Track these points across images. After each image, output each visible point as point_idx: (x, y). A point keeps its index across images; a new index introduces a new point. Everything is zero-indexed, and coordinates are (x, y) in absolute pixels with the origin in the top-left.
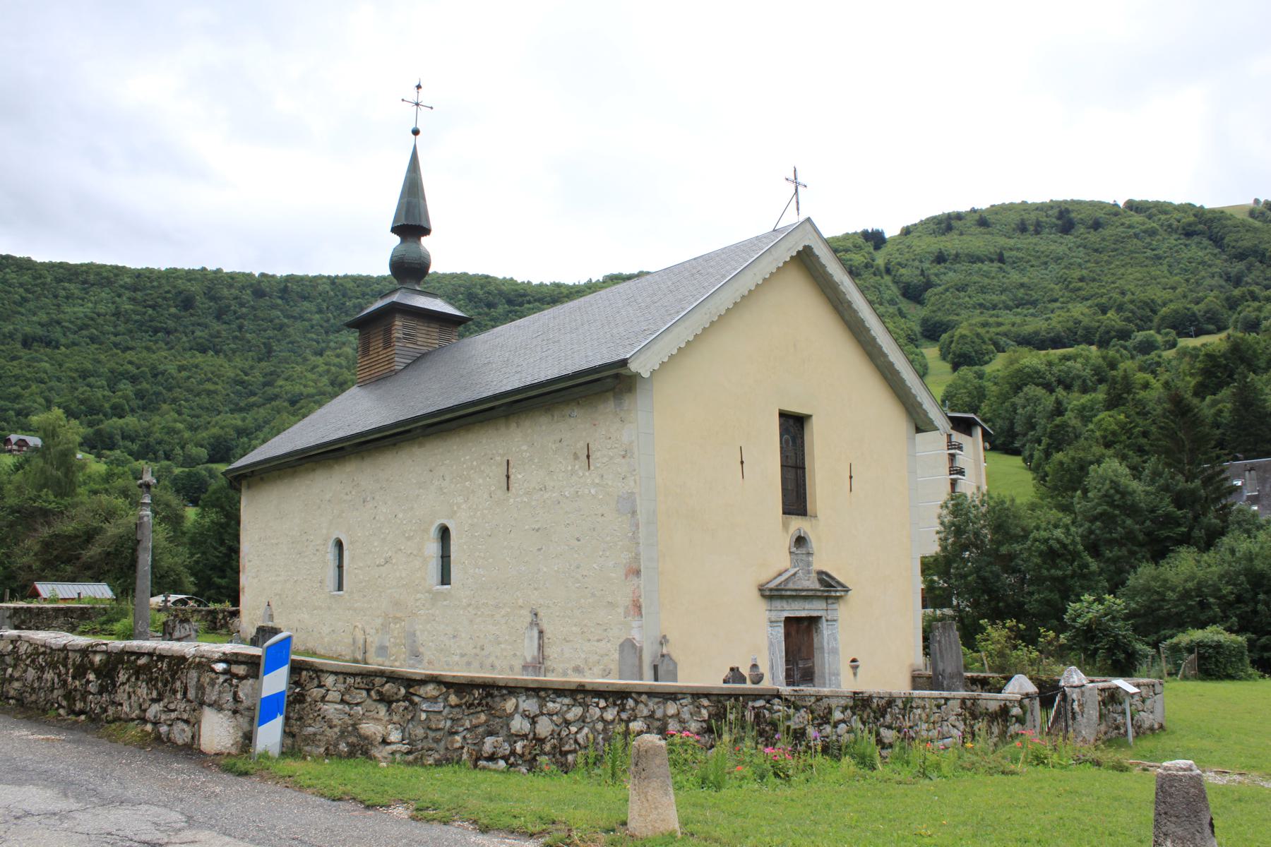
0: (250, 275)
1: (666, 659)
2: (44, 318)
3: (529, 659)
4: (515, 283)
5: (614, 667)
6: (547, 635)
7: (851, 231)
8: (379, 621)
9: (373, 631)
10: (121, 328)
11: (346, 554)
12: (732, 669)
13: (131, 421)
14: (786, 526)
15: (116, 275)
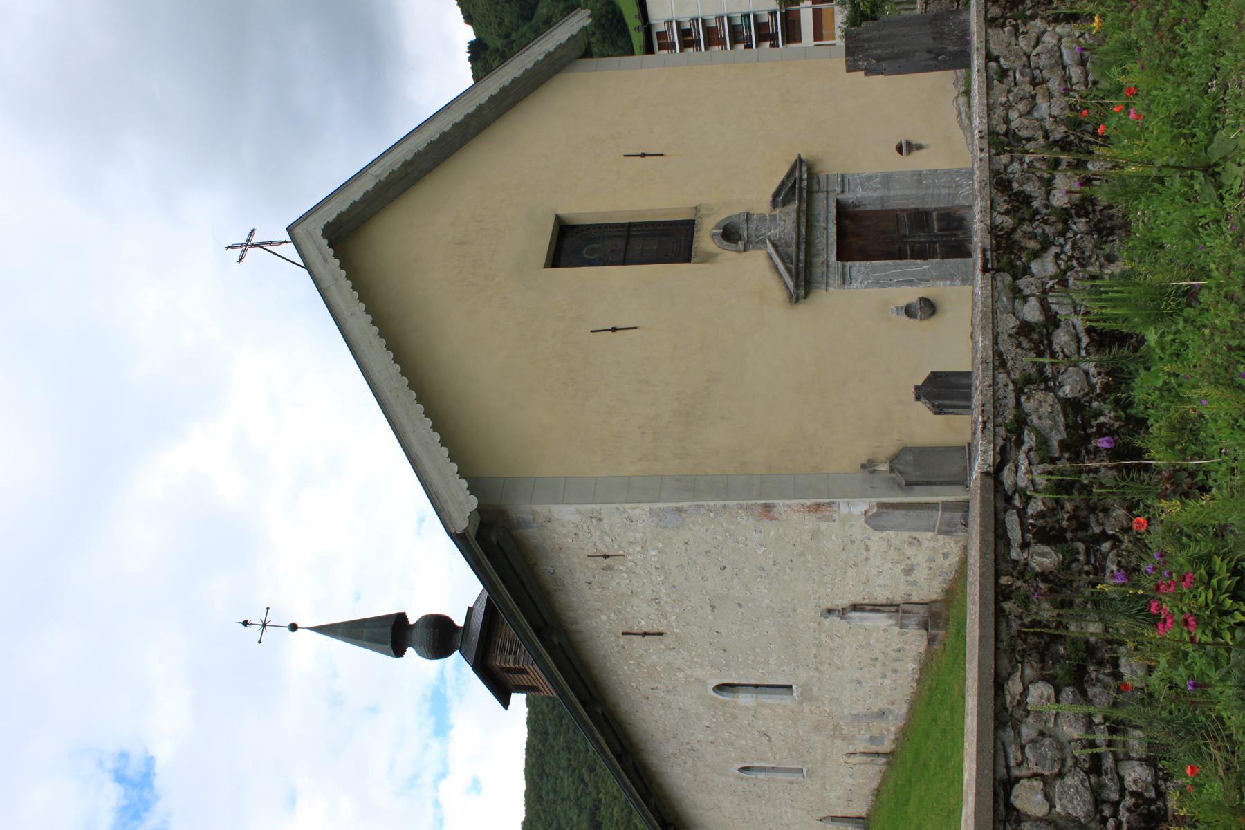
2: (573, 813)
6: (858, 600)
11: (756, 764)
12: (918, 398)
14: (708, 258)
15: (534, 750)
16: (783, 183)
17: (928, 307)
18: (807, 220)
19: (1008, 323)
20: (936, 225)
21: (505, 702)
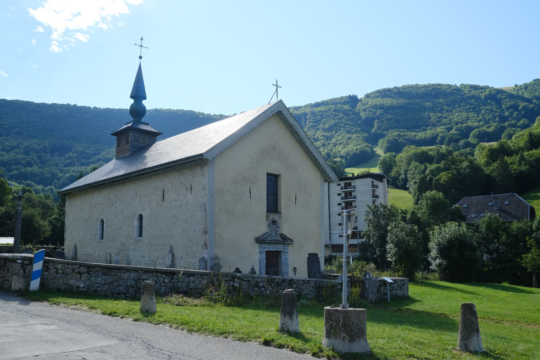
4: (204, 114)
5: (197, 267)
7: (344, 96)
8: (116, 251)
9: (114, 255)
11: (105, 225)
16: (286, 237)
18: (277, 243)
19: (259, 280)
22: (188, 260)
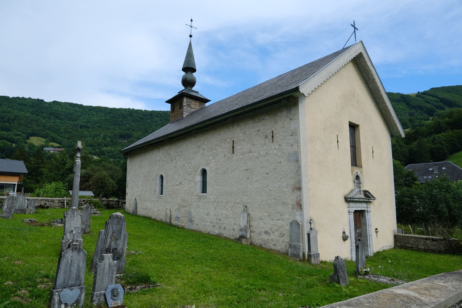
0: (142, 110)
1: (313, 230)
2: (85, 120)
3: (243, 226)
8: (177, 207)
9: (174, 211)
10: (107, 124)
11: (164, 180)
13: (109, 148)
14: (352, 171)
17: (345, 238)
20: (114, 214)
21: (168, 102)
22: (272, 222)
